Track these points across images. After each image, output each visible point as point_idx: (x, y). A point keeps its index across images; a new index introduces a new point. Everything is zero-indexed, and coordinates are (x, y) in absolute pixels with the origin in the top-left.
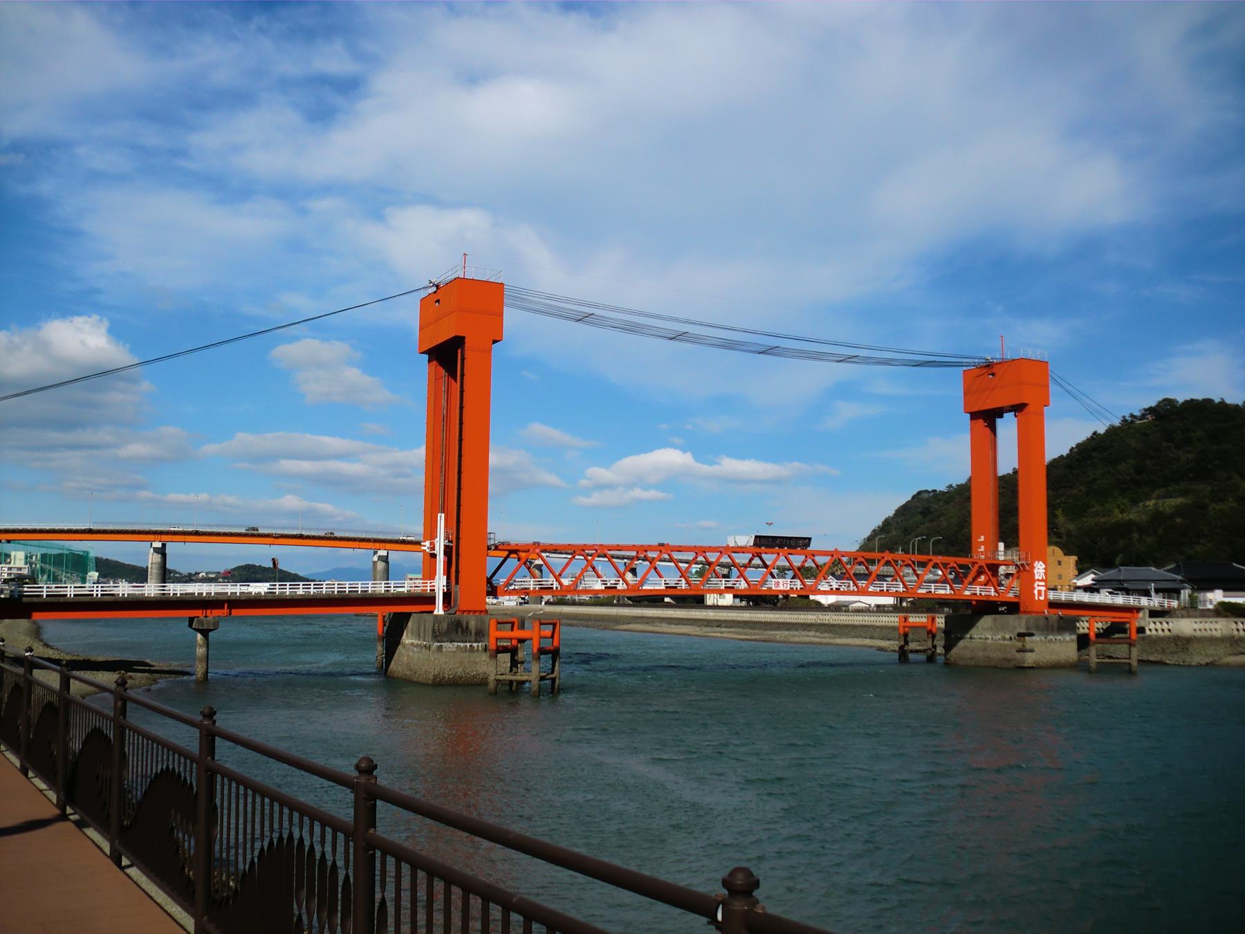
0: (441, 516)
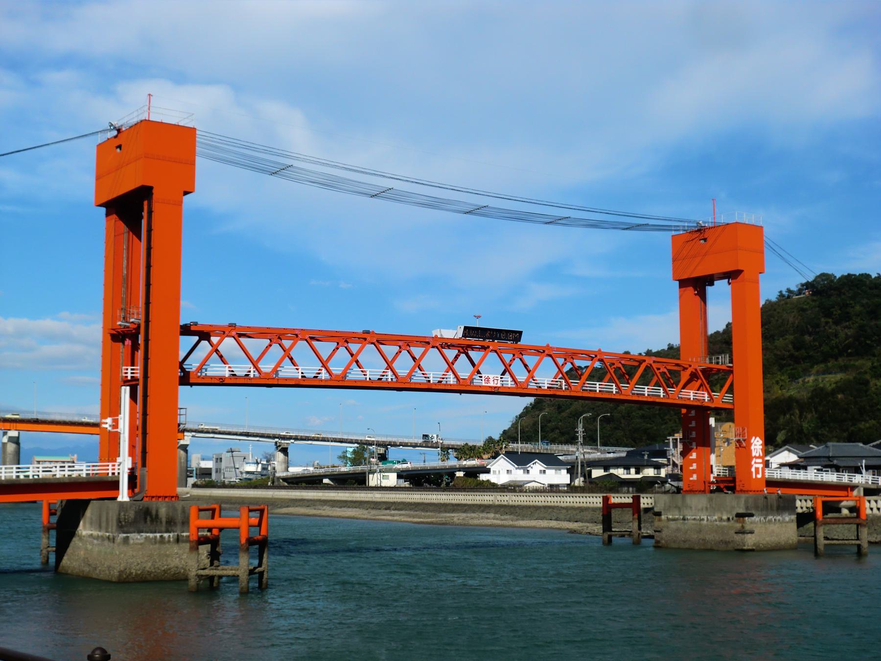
0: (125, 390)
